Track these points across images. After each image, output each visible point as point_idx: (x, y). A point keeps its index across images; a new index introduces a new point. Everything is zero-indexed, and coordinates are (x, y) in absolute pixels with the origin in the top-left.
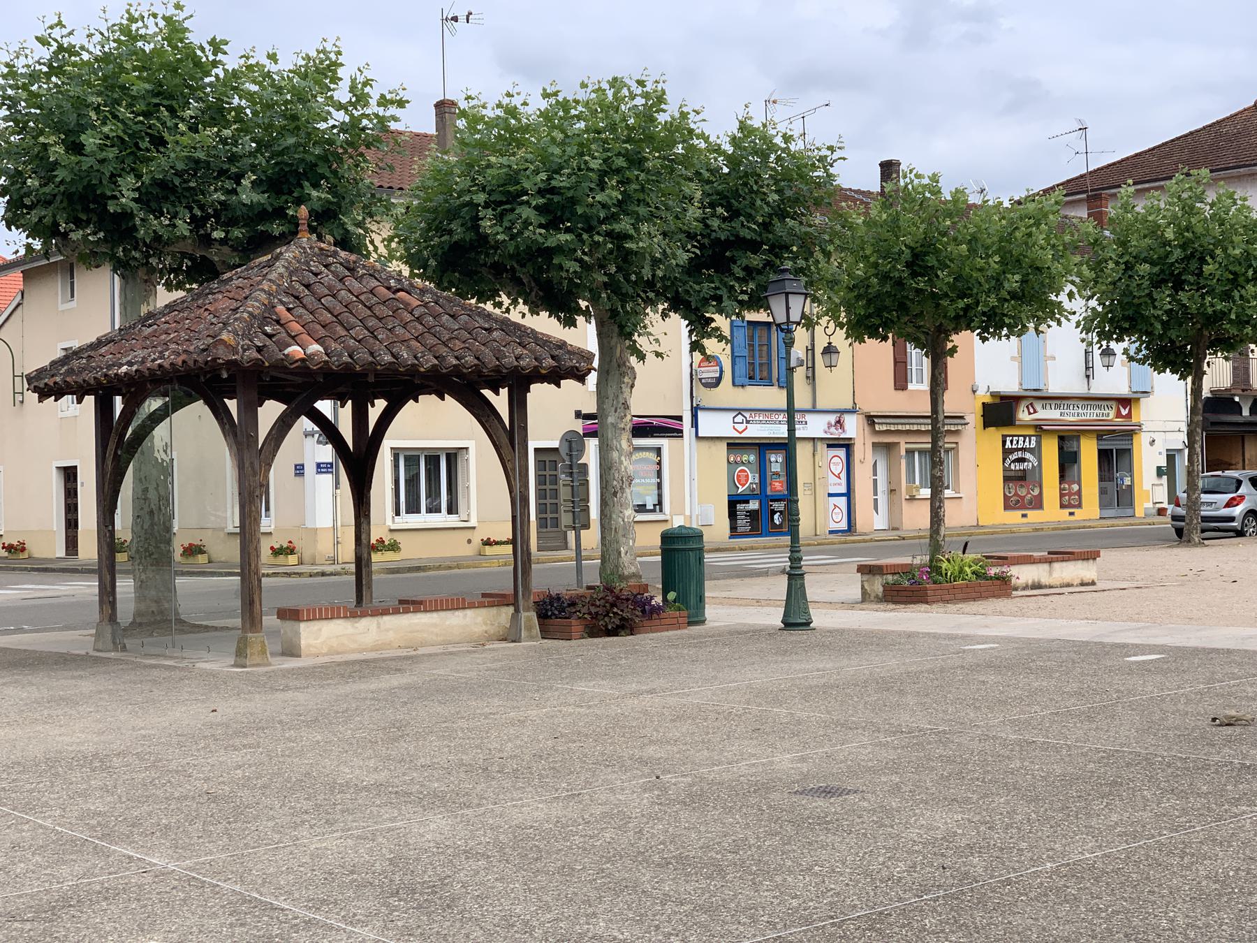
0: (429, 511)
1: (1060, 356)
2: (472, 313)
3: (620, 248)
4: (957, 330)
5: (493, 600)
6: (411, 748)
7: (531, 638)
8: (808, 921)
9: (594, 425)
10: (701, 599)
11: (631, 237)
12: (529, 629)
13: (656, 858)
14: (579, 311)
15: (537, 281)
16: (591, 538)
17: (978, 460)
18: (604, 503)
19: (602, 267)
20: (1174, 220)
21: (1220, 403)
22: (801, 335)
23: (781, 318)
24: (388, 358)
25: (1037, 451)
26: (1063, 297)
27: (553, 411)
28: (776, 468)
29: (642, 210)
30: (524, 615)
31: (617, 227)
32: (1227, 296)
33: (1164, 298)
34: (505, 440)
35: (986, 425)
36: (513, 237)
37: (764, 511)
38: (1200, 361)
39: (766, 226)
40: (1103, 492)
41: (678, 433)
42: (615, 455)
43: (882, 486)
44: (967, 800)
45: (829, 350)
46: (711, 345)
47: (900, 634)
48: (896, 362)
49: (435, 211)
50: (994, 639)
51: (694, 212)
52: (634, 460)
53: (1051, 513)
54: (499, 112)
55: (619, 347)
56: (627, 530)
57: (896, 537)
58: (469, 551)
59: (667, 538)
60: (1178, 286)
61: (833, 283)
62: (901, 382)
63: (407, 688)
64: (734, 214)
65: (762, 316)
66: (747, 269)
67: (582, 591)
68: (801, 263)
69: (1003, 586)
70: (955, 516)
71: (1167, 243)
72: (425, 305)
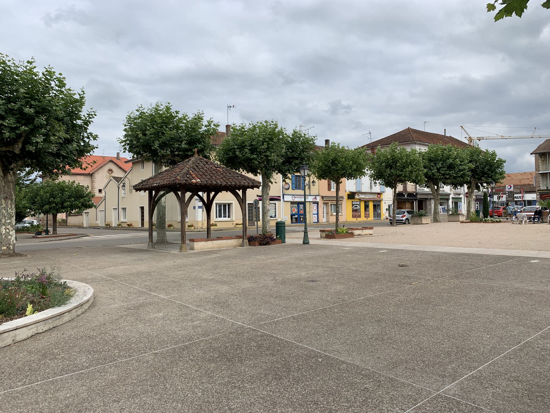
1: (365, 184)
3: (267, 158)
5: (238, 237)
9: (261, 198)
10: (285, 237)
17: (346, 207)
18: (263, 215)
20: (390, 153)
21: (400, 194)
22: (307, 178)
23: (303, 175)
24: (215, 183)
25: (359, 205)
26: (365, 170)
27: (252, 195)
28: (301, 208)
29: (272, 150)
30: (245, 241)
31: (267, 154)
33: (388, 171)
36: (243, 156)
37: (299, 217)
38: (396, 185)
39: (300, 154)
40: (374, 214)
41: (280, 200)
44: (344, 283)
45: (313, 182)
51: (284, 151)
52: (270, 206)
53: (363, 219)
56: (268, 222)
57: (328, 224)
59: (277, 223)
60: (391, 169)
61: (315, 167)
62: (329, 189)
63: (218, 257)
64: (293, 151)
65: (298, 174)
66: (296, 164)
68: (307, 162)
69: (352, 235)
70: (341, 219)
71: (388, 159)
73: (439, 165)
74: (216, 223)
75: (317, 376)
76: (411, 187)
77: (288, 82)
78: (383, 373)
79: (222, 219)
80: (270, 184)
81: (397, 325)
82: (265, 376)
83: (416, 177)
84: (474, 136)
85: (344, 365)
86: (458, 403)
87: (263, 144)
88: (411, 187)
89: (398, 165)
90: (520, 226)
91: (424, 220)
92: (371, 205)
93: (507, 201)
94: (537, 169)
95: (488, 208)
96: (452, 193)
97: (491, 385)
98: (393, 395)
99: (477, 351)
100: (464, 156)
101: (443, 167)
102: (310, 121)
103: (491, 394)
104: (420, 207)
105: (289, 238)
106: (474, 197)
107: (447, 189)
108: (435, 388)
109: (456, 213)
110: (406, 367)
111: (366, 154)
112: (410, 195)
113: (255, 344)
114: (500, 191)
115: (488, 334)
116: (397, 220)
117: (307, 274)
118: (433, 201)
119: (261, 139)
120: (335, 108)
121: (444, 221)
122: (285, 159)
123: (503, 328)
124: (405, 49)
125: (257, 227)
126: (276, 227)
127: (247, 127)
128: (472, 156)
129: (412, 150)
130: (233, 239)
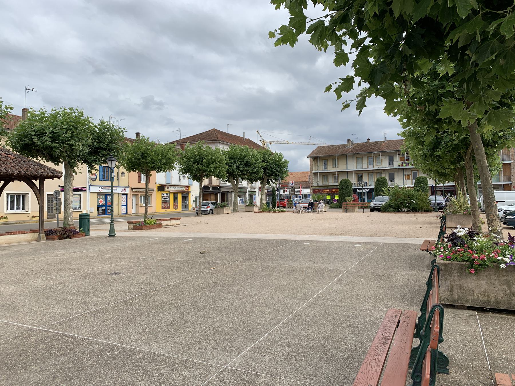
0: (17, 209)
1: (174, 177)
2: (29, 161)
3: (71, 148)
4: (152, 170)
5: (33, 231)
6: (6, 270)
7: (44, 240)
8: (109, 303)
9: (63, 188)
10: (89, 230)
11: (74, 145)
12: (43, 238)
13: (72, 292)
14: (60, 162)
15: (49, 154)
16: (61, 216)
17: (156, 198)
18: (65, 207)
19: (66, 152)
20: (197, 150)
21: (206, 187)
22: (116, 170)
23: (110, 166)
24: (5, 171)
26: (174, 165)
27: (51, 186)
28: (109, 199)
29: (77, 139)
30: (41, 235)
31: (70, 143)
32: (207, 167)
33: (195, 166)
34: (38, 192)
36: (42, 143)
37: (105, 209)
38: (202, 179)
39: (108, 145)
40: (182, 205)
41: (85, 191)
42: (68, 196)
43: (134, 204)
44: (148, 273)
45: (123, 173)
46: (93, 171)
47: (136, 237)
49: (21, 135)
50: (157, 237)
51: (90, 141)
52: (74, 198)
53: (172, 210)
54: (39, 113)
55: (70, 171)
56: (71, 214)
57: (137, 215)
58: (28, 219)
59: (80, 216)
60: (198, 164)
61: (124, 159)
62: (139, 181)
63: (7, 254)
64: (100, 142)
65: (106, 165)
66: (103, 155)
67: (58, 228)
68: (116, 154)
69: (160, 226)
70: (150, 210)
71: (195, 155)
72: (16, 158)
73: (238, 163)
74: (7, 215)
75: (112, 370)
76: (215, 181)
77: (99, 71)
78: (178, 357)
79: (15, 211)
80: (74, 174)
81: (194, 309)
82: (53, 380)
83: (220, 173)
84: (267, 140)
85: (141, 355)
86: (241, 373)
87: (66, 133)
88: (215, 181)
89: (204, 161)
90: (298, 215)
91: (226, 210)
92: (180, 197)
93: (290, 194)
94: (311, 169)
95: (275, 200)
96: (249, 187)
97: (269, 352)
98: (186, 376)
99: (259, 324)
100: (258, 156)
102: (121, 113)
103: (267, 361)
104: (223, 199)
105: (94, 230)
106: (266, 191)
107: (245, 183)
108: (223, 363)
109: (252, 204)
110: (199, 348)
111: (176, 150)
112: (214, 188)
113: (44, 347)
114: (285, 186)
115: (269, 309)
116: (202, 211)
117: (111, 266)
118: (233, 194)
119: (65, 127)
120: (148, 103)
121: (242, 211)
122: (92, 149)
123: (281, 302)
124: (212, 57)
125: (58, 220)
126: (80, 219)
127: (48, 112)
128: (264, 157)
129: (217, 149)
130: (27, 233)
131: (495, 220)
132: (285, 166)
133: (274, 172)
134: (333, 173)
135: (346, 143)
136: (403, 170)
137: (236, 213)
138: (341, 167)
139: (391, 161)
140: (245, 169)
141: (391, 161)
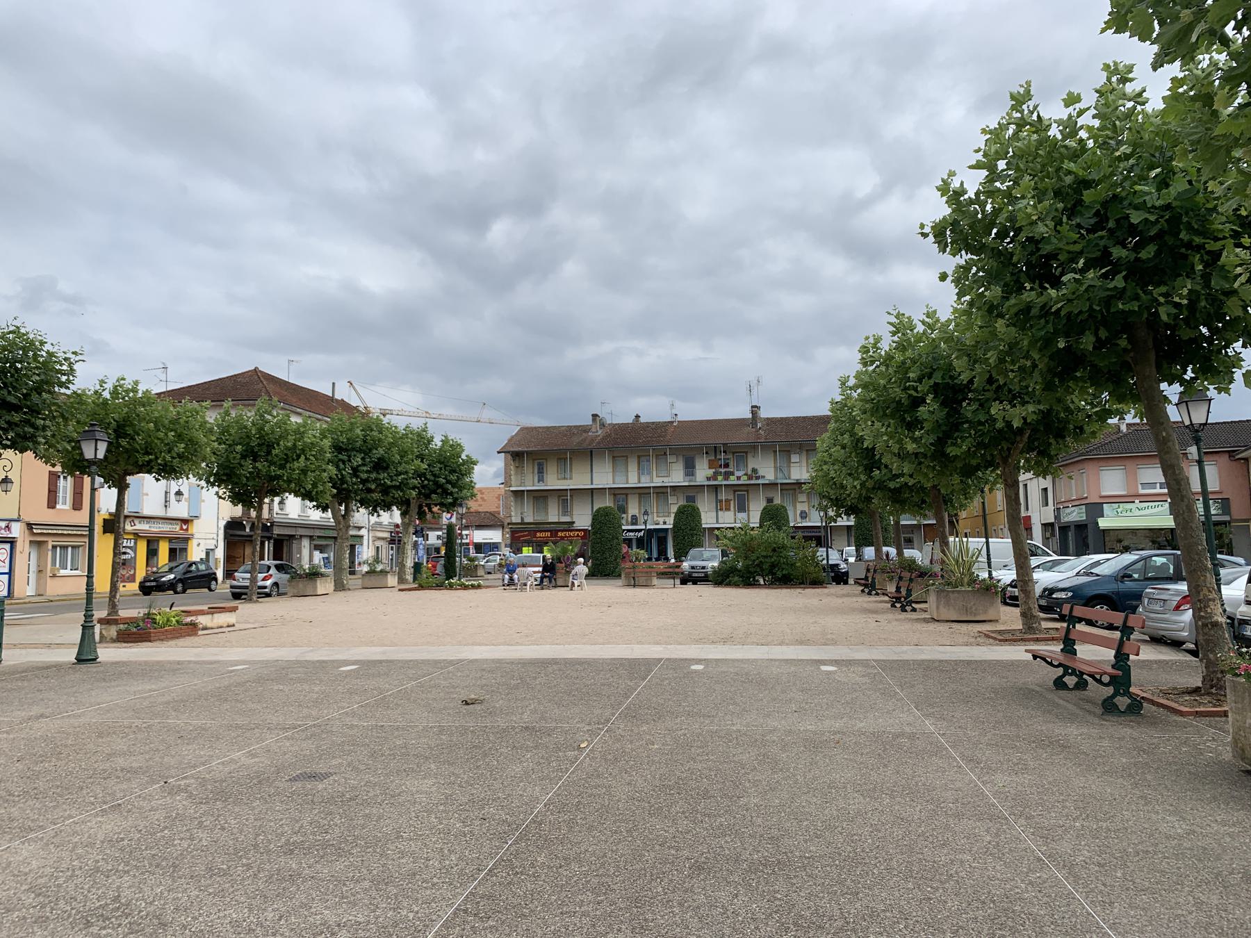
25: (134, 549)
32: (282, 467)
33: (248, 465)
35: (105, 532)
39: (26, 396)
43: (33, 568)
48: (49, 491)
60: (255, 460)
62: (52, 503)
69: (193, 629)
73: (357, 461)
83: (315, 485)
92: (164, 549)
94: (507, 483)
101: (364, 465)
124: (222, 191)
131: (1214, 600)
132: (469, 472)
133: (441, 486)
134: (560, 494)
135: (588, 421)
136: (716, 488)
137: (342, 594)
138: (579, 479)
139: (690, 468)
140: (373, 476)
141: (690, 468)
